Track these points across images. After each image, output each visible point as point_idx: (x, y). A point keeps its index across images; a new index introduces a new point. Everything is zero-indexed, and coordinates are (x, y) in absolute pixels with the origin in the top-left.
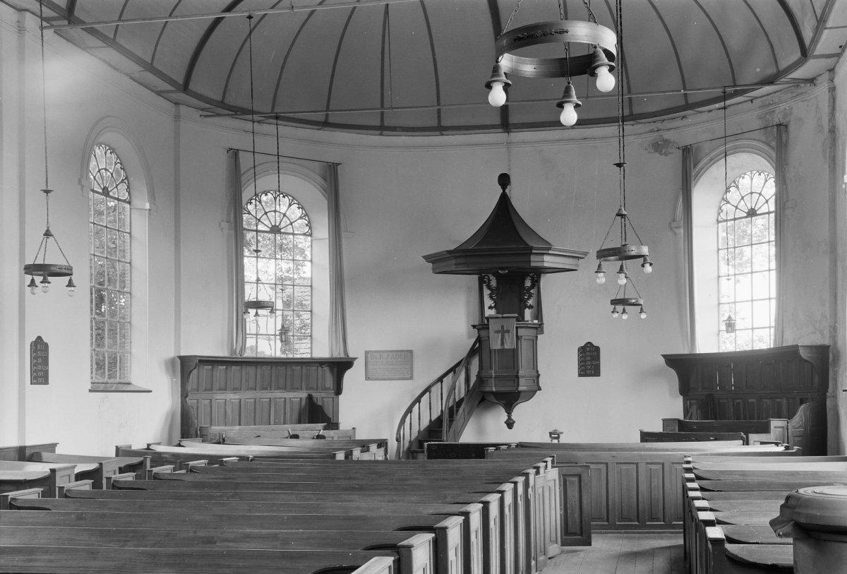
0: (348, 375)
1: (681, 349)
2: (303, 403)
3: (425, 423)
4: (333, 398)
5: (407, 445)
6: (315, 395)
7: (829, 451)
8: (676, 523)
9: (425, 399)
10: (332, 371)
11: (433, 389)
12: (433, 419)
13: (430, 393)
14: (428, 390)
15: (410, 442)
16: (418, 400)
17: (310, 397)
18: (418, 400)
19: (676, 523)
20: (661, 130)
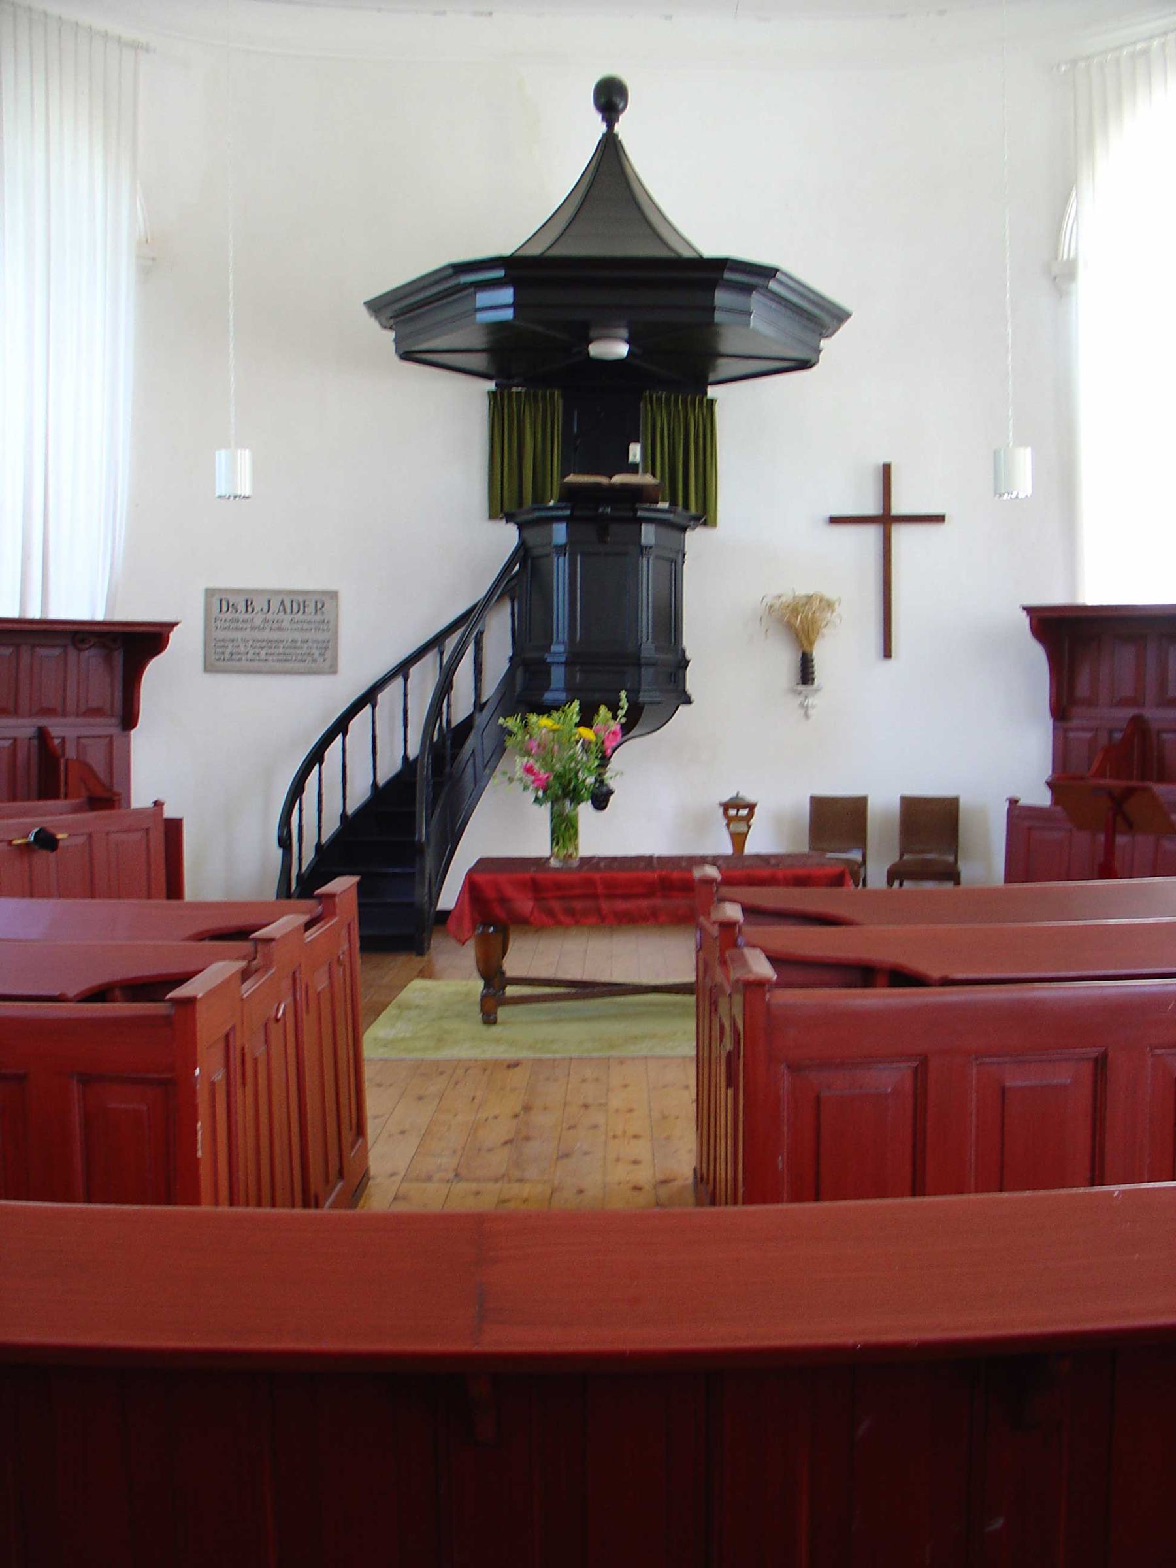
0: (155, 673)
1: (1055, 596)
2: (21, 755)
3: (360, 793)
4: (111, 737)
5: (309, 855)
6: (58, 728)
7: (1006, 885)
8: (449, 848)
9: (359, 724)
10: (108, 660)
11: (382, 697)
12: (381, 781)
13: (374, 707)
14: (369, 697)
15: (319, 847)
16: (340, 727)
17: (43, 735)
18: (340, 727)
19: (449, 848)
20: (605, 1158)
